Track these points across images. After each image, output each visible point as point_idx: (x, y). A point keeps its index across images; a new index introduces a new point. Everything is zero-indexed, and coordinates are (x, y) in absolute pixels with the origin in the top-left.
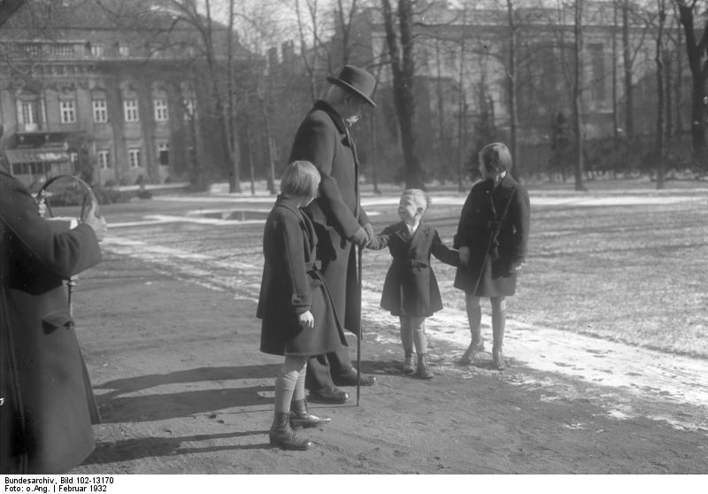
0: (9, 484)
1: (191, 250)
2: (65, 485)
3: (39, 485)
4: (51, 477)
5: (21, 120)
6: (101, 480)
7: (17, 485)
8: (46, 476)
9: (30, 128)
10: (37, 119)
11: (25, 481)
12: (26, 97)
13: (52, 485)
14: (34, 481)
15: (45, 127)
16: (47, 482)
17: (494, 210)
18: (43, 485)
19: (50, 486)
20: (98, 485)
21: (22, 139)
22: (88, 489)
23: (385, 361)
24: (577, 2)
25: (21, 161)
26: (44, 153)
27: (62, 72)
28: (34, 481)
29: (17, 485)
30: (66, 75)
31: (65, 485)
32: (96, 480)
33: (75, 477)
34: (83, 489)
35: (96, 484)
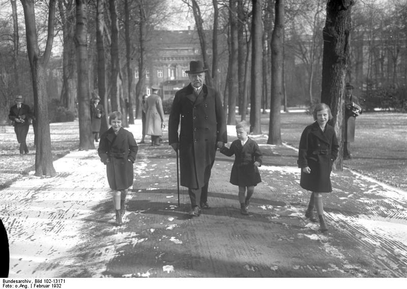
0: (5, 283)
1: (341, 84)
2: (38, 284)
3: (23, 284)
5: (169, 76)
6: (58, 281)
7: (10, 284)
9: (172, 78)
10: (175, 76)
11: (14, 281)
12: (171, 68)
13: (30, 284)
14: (20, 282)
15: (177, 78)
16: (27, 282)
18: (24, 284)
19: (29, 285)
20: (56, 284)
21: (169, 82)
22: (51, 287)
24: (236, 19)
25: (167, 90)
26: (175, 87)
27: (169, 60)
28: (20, 282)
29: (10, 284)
30: (174, 60)
31: (38, 284)
32: (55, 281)
34: (48, 286)
35: (55, 283)
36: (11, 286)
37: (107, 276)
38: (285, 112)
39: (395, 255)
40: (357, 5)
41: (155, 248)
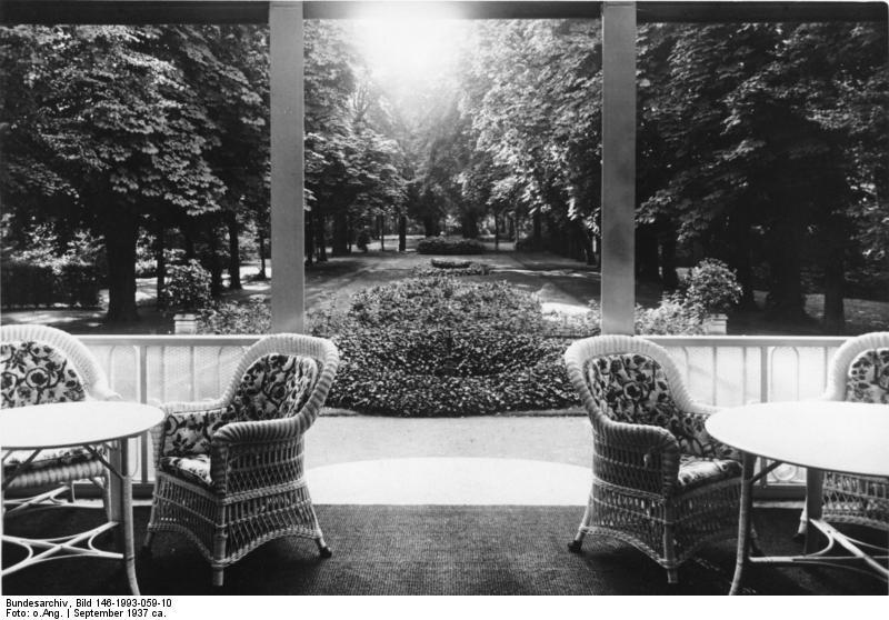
0: (11, 607)
2: (81, 609)
3: (50, 609)
4: (64, 598)
7: (22, 609)
8: (58, 598)
11: (31, 603)
13: (66, 609)
14: (43, 604)
16: (60, 605)
17: (660, 252)
18: (54, 609)
19: (62, 610)
22: (125, 614)
23: (713, 316)
28: (43, 604)
29: (22, 609)
33: (94, 598)
36: (24, 614)
37: (391, 509)
38: (360, 251)
39: (383, 225)
40: (484, 119)
41: (673, 219)
